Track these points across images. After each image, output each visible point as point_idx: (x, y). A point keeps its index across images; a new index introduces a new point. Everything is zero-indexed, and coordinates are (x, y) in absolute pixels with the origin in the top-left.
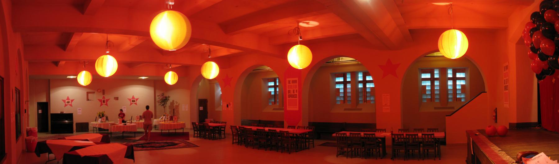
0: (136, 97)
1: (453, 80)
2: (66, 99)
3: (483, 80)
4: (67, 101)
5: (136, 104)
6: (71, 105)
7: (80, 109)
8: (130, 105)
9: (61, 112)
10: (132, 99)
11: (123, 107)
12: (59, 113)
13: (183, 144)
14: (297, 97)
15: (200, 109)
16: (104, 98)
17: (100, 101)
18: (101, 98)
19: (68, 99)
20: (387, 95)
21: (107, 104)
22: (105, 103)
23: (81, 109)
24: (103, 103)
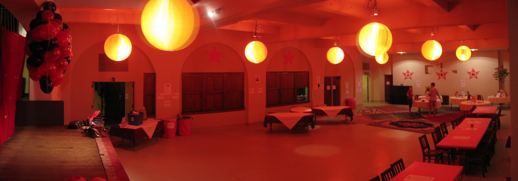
0: (476, 70)
4: (406, 74)
5: (476, 77)
6: (410, 78)
7: (419, 82)
9: (401, 85)
11: (462, 81)
12: (400, 85)
14: (259, 81)
16: (442, 71)
17: (438, 74)
18: (439, 71)
19: (408, 72)
21: (444, 78)
23: (465, 81)
24: (440, 77)
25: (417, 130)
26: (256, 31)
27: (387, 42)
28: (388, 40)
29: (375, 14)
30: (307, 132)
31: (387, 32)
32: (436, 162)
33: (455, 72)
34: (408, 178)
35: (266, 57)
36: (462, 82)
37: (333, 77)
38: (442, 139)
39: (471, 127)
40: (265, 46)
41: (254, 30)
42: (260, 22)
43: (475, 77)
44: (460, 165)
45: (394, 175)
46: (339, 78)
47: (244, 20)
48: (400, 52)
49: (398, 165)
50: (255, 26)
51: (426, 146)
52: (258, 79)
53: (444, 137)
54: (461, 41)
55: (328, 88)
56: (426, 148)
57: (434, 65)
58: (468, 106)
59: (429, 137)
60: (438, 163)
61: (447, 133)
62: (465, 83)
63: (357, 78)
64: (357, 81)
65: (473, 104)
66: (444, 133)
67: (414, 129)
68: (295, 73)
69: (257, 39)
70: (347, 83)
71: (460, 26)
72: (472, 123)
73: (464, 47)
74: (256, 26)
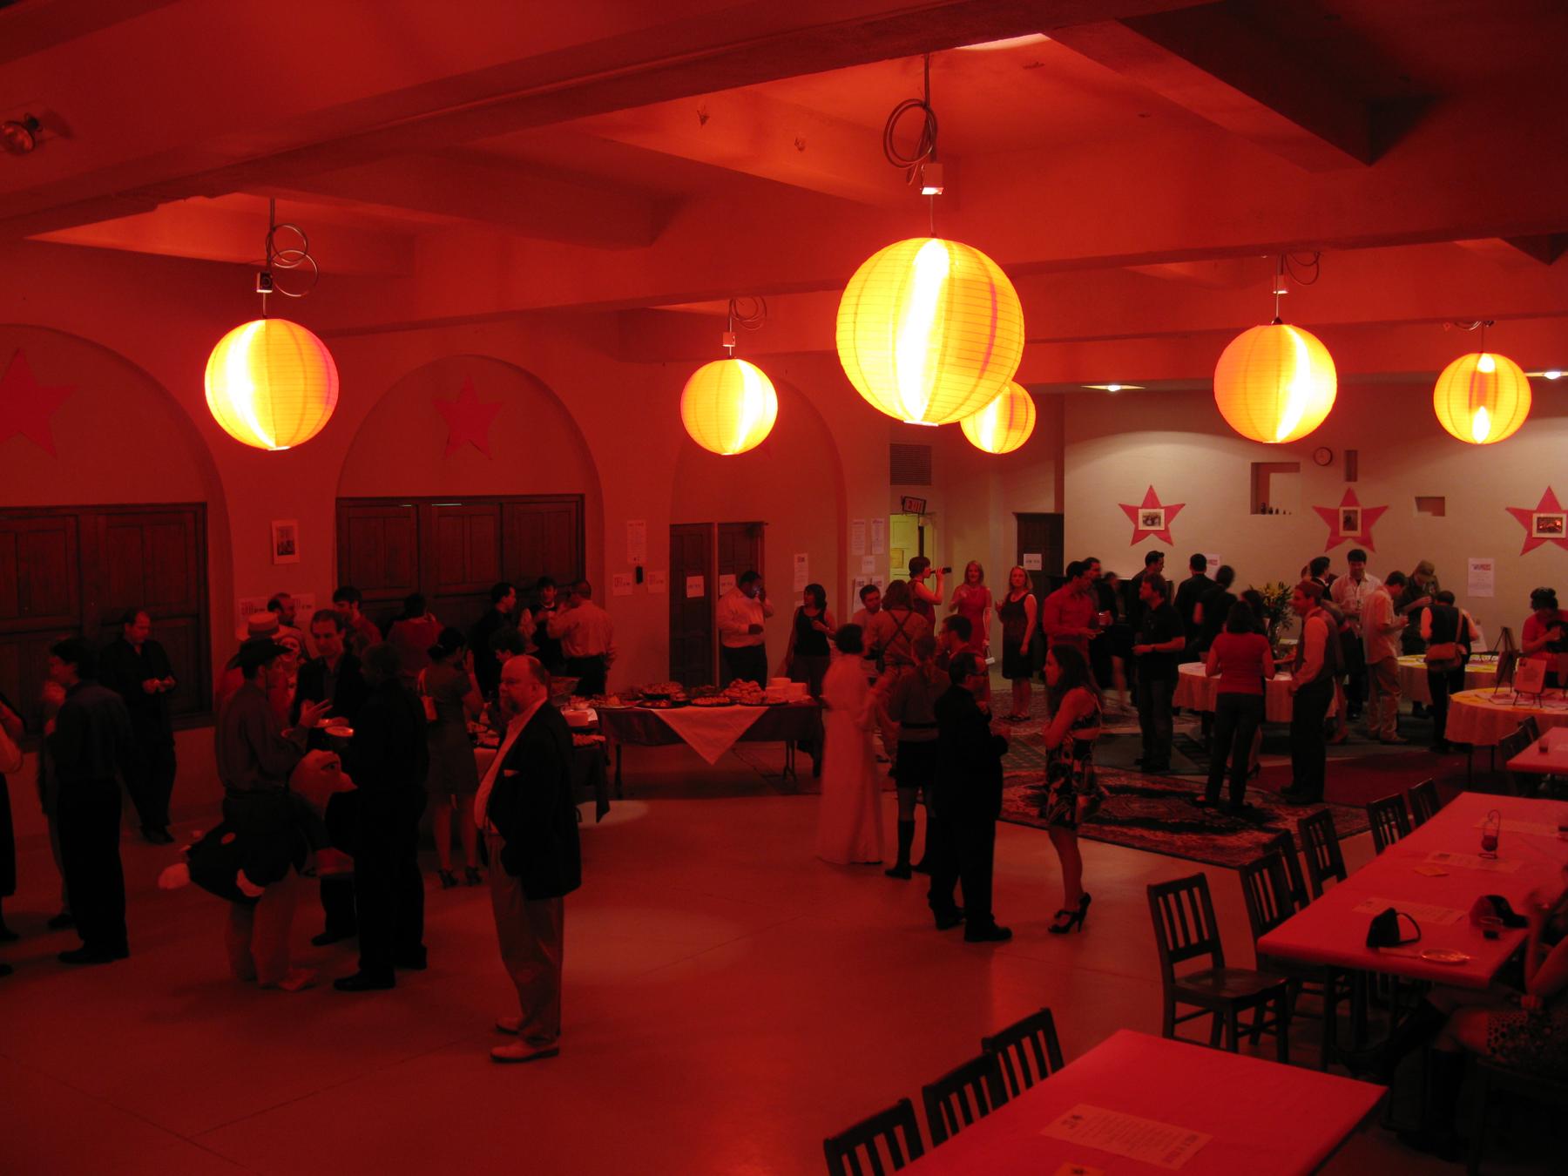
2: (1140, 503)
8: (1527, 549)
10: (1145, 506)
11: (1472, 561)
13: (1255, 827)
14: (292, 552)
15: (699, 580)
16: (1350, 498)
17: (1328, 515)
18: (1334, 502)
19: (1151, 499)
20: (639, 525)
22: (1358, 533)
23: (1489, 561)
24: (1342, 533)
25: (1178, 839)
26: (270, 261)
27: (995, 350)
28: (997, 341)
29: (929, 191)
31: (993, 290)
32: (1223, 1044)
34: (1065, 1122)
35: (329, 414)
36: (1471, 569)
37: (719, 524)
38: (1305, 903)
40: (325, 349)
41: (258, 256)
42: (287, 206)
43: (1555, 540)
44: (1356, 1070)
45: (1000, 1099)
46: (753, 531)
47: (197, 194)
49: (1026, 1042)
50: (267, 231)
51: (1328, 863)
52: (291, 544)
53: (1318, 892)
54: (1471, 323)
55: (695, 587)
56: (1190, 951)
58: (1492, 715)
59: (1226, 889)
60: (1233, 1048)
61: (1338, 870)
64: (856, 549)
65: (1526, 706)
66: (1320, 876)
69: (272, 310)
72: (1491, 827)
73: (1488, 363)
74: (273, 229)
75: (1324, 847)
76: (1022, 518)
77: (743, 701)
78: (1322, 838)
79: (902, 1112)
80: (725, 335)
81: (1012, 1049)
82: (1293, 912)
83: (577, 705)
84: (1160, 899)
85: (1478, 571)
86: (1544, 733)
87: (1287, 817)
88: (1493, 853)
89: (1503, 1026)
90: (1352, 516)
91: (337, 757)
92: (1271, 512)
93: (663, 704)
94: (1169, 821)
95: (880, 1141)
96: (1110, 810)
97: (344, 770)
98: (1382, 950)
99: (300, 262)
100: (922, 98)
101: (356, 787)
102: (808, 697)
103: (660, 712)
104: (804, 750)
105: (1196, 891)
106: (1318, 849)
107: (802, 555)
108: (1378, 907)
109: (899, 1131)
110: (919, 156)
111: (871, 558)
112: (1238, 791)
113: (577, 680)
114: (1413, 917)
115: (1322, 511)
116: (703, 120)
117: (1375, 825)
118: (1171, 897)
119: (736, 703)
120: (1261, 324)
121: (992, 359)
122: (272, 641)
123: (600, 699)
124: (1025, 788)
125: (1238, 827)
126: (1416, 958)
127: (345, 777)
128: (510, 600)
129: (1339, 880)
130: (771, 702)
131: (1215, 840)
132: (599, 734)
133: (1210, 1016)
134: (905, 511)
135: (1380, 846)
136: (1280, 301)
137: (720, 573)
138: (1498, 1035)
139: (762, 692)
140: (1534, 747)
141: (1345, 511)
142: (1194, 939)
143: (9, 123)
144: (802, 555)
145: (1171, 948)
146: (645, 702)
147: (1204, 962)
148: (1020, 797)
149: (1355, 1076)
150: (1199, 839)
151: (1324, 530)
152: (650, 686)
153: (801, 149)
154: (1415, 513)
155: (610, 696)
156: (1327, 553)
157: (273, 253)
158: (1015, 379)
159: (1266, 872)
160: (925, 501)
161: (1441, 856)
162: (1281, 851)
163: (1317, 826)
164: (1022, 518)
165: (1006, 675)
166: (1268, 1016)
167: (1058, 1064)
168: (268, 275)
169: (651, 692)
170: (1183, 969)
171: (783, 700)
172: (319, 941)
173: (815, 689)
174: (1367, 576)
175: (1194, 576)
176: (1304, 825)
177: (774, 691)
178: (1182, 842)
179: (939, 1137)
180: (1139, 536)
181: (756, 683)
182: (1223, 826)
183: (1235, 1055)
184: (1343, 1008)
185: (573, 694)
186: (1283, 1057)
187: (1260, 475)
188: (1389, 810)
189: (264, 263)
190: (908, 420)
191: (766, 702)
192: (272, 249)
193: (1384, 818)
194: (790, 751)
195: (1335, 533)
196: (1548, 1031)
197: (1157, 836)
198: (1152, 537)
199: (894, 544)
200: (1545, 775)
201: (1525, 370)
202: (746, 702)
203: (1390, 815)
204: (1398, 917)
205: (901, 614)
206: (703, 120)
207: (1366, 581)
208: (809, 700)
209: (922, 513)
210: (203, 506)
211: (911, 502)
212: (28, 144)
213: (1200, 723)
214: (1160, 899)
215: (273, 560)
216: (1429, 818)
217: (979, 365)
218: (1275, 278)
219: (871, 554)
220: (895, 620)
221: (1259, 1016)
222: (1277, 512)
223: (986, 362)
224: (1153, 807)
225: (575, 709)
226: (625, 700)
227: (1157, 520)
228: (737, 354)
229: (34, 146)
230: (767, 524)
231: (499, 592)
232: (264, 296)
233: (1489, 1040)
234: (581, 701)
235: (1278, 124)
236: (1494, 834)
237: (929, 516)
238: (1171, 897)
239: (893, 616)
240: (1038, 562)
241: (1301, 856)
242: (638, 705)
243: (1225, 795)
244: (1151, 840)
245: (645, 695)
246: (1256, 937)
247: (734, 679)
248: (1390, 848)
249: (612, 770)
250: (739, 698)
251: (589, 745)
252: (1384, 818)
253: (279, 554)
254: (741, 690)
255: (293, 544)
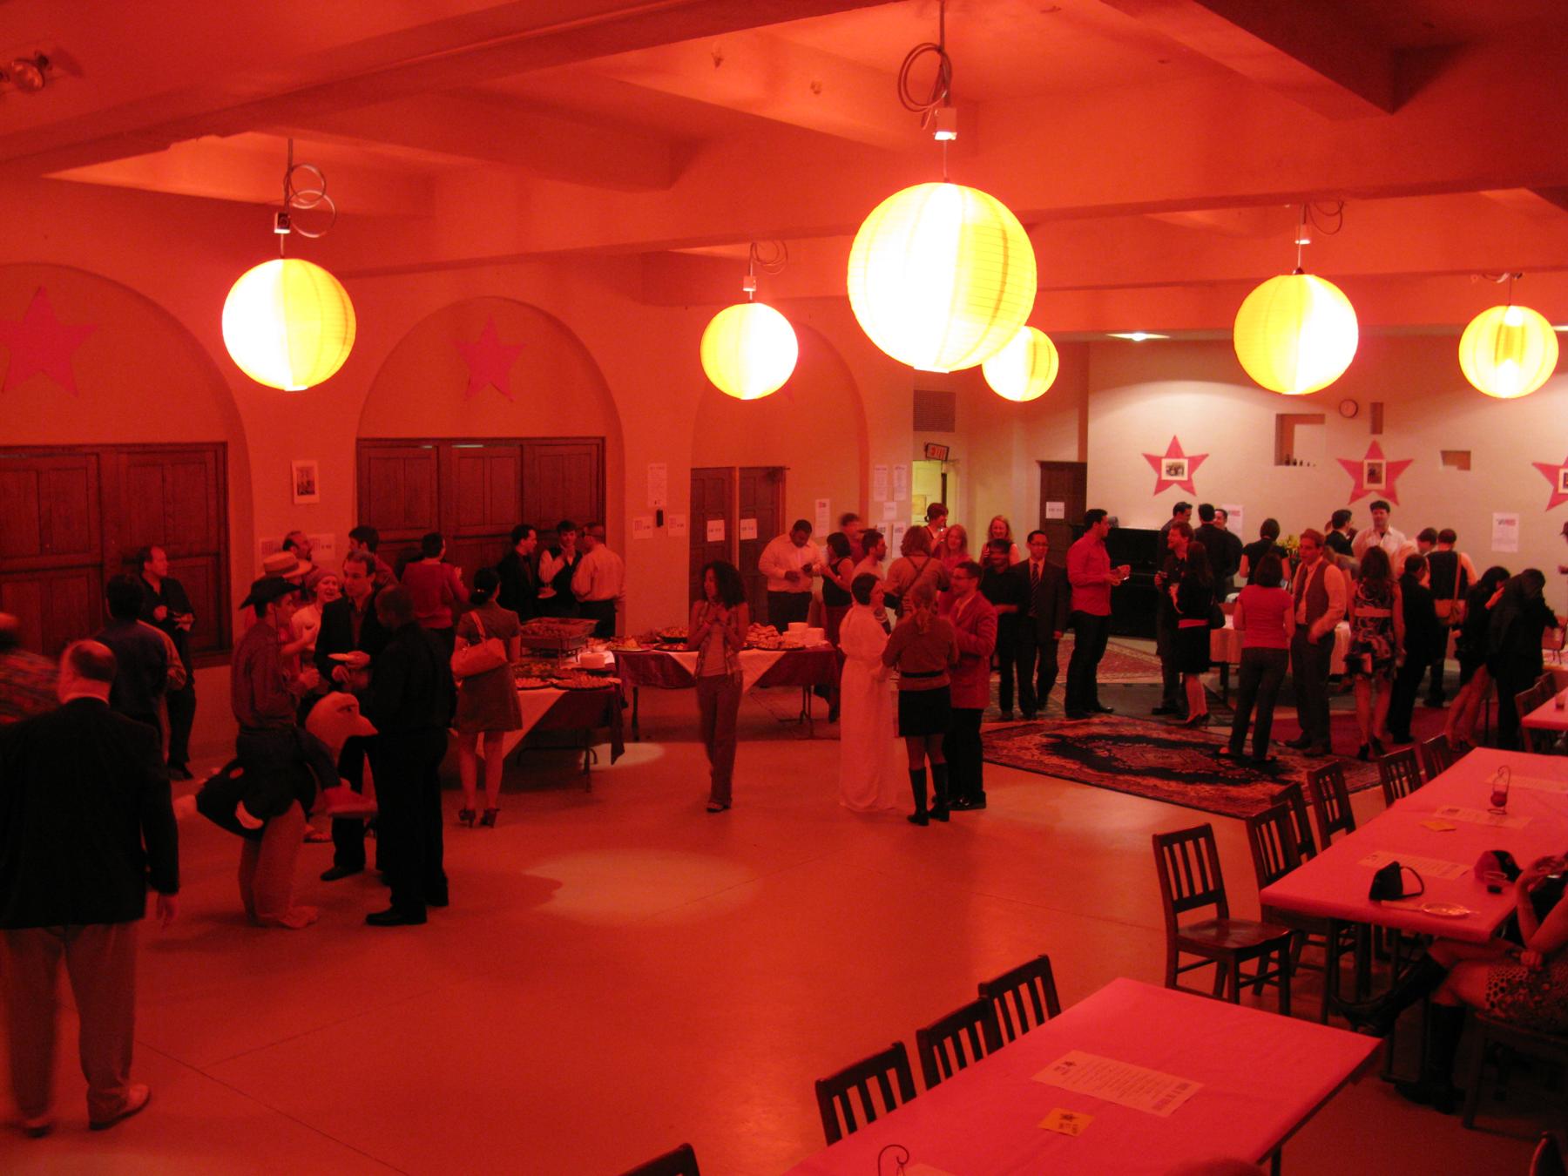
1: (725, 541)
3: (225, 524)
10: (1169, 455)
11: (1497, 516)
13: (1269, 778)
14: (313, 493)
16: (1375, 451)
17: (1353, 468)
18: (1359, 454)
19: (1175, 449)
20: (660, 468)
22: (1382, 486)
24: (1367, 486)
25: (1192, 790)
26: (288, 201)
29: (943, 136)
30: (583, 782)
32: (1225, 995)
33: (1460, 459)
35: (346, 354)
36: (1495, 524)
37: (741, 469)
38: (1312, 854)
39: (1491, 806)
41: (276, 196)
42: (312, 147)
44: (1355, 1022)
45: (995, 1044)
46: (775, 475)
47: (208, 133)
48: (1131, 331)
49: (1024, 989)
51: (1337, 816)
53: (1326, 843)
54: (1499, 275)
56: (1194, 902)
57: (1331, 417)
59: (1230, 836)
60: (1235, 999)
61: (1348, 823)
62: (1514, 531)
63: (878, 479)
66: (1328, 829)
67: (1173, 786)
68: (523, 447)
69: (294, 250)
70: (823, 505)
71: (1487, 193)
72: (1501, 785)
74: (291, 169)
75: (1334, 802)
76: (1046, 466)
77: (761, 645)
78: (1332, 792)
79: (896, 1055)
80: (746, 280)
81: (1009, 996)
82: (1299, 864)
83: (594, 647)
84: (1166, 849)
85: (1502, 526)
86: (1562, 690)
87: (1302, 769)
88: (1502, 808)
89: (1502, 980)
90: (1376, 468)
91: (352, 699)
92: (1295, 464)
93: (680, 648)
94: (1184, 772)
95: (873, 1084)
96: (1125, 759)
97: (363, 713)
98: (1384, 902)
99: (318, 202)
100: (937, 41)
101: (376, 732)
102: (825, 642)
103: (679, 656)
104: (821, 696)
105: (1202, 841)
106: (1327, 803)
107: (823, 501)
108: (1382, 860)
109: (892, 1074)
110: (934, 99)
111: (893, 504)
112: (1262, 742)
113: (595, 622)
114: (1417, 872)
115: (1346, 464)
116: (718, 62)
117: (1386, 781)
118: (1176, 847)
119: (753, 648)
120: (1283, 274)
121: (1003, 305)
122: (281, 578)
123: (617, 642)
124: (1041, 736)
125: (1252, 779)
126: (1417, 911)
127: (364, 720)
128: (528, 544)
129: (1348, 832)
130: (787, 647)
131: (1228, 791)
132: (615, 676)
133: (1214, 966)
134: (927, 458)
135: (1390, 798)
136: (1303, 253)
137: (742, 517)
138: (1498, 989)
139: (779, 637)
140: (1550, 704)
141: (1369, 464)
142: (1199, 890)
143: (19, 61)
144: (823, 501)
145: (1175, 897)
146: (663, 645)
147: (1209, 912)
148: (1035, 745)
149: (1354, 1030)
150: (1212, 789)
151: (1349, 483)
152: (668, 629)
153: (817, 92)
154: (1441, 467)
155: (628, 639)
156: (1352, 505)
157: (291, 193)
158: (1031, 322)
159: (1273, 823)
160: (948, 448)
161: (1449, 810)
162: (1290, 803)
163: (1328, 779)
164: (1046, 466)
165: (554, 588)
166: (1272, 967)
167: (1055, 1010)
168: (286, 216)
169: (668, 636)
170: (1187, 919)
171: (800, 645)
172: (327, 877)
173: (832, 635)
174: (1391, 529)
175: (1203, 525)
176: (1314, 777)
177: (792, 636)
178: (1195, 792)
179: (932, 1080)
180: (1162, 486)
181: (773, 628)
182: (1237, 777)
183: (1235, 1006)
184: (1347, 961)
185: (591, 636)
186: (1285, 1010)
187: (1285, 425)
188: (1400, 763)
189: (282, 203)
190: (918, 367)
191: (783, 647)
192: (290, 190)
193: (1394, 772)
194: (807, 695)
195: (1359, 486)
196: (1546, 986)
197: (1170, 787)
198: (1175, 488)
199: (917, 490)
200: (1562, 732)
201: (1553, 323)
202: (764, 646)
203: (1402, 770)
204: (1402, 871)
205: (920, 561)
206: (718, 62)
207: (1389, 534)
208: (826, 645)
209: (946, 460)
210: (224, 445)
211: (934, 449)
212: (38, 81)
213: (1218, 675)
214: (1166, 849)
215: (293, 501)
216: (1440, 772)
217: (991, 311)
218: (1297, 228)
219: (893, 500)
220: (915, 567)
221: (1263, 967)
222: (1301, 463)
223: (997, 309)
224: (1168, 757)
225: (593, 651)
226: (644, 643)
227: (1180, 471)
228: (757, 298)
229: (44, 85)
230: (789, 469)
231: (520, 533)
232: (282, 238)
233: (1488, 995)
234: (599, 644)
235: (1297, 70)
236: (1504, 791)
237: (951, 463)
238: (1176, 847)
239: (912, 563)
240: (1061, 510)
241: (1310, 810)
242: (655, 648)
243: (1248, 749)
244: (1167, 791)
245: (664, 638)
246: (1260, 889)
247: (751, 623)
248: (1399, 802)
249: (628, 712)
250: (757, 643)
251: (605, 687)
252: (1394, 772)
253: (298, 494)
254: (759, 635)
255: (314, 485)
